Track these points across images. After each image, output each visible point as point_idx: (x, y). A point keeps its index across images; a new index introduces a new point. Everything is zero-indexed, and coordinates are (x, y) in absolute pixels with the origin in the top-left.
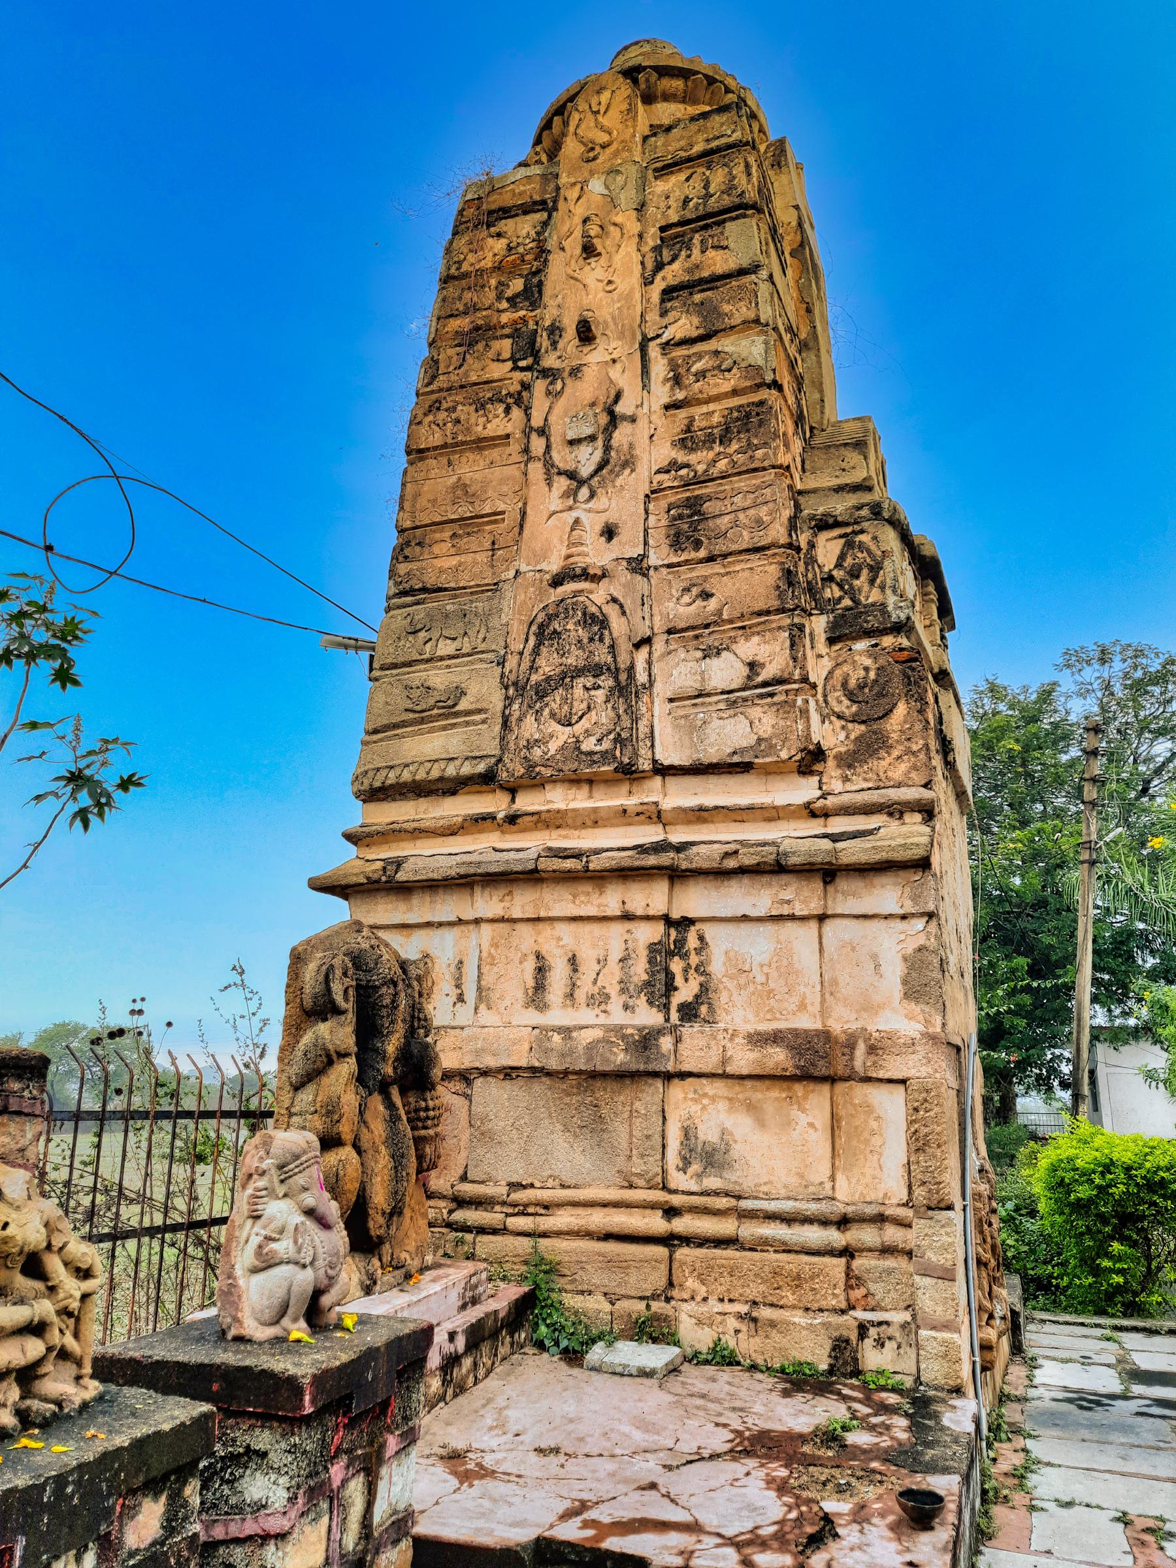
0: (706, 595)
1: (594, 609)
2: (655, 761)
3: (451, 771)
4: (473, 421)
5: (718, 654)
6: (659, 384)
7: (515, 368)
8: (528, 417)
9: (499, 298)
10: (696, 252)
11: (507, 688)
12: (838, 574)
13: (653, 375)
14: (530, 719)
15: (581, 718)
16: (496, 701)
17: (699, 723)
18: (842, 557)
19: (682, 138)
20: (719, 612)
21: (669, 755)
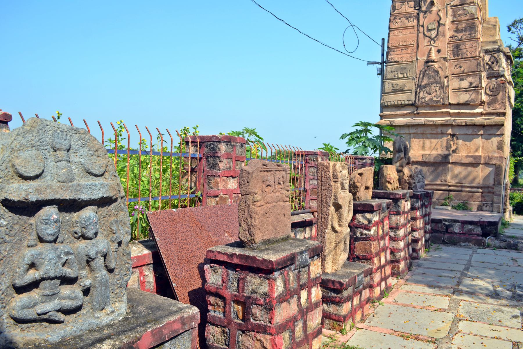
0: (461, 67)
3: (403, 102)
12: (490, 63)
13: (448, 14)
16: (414, 89)
18: (490, 59)
20: (464, 71)
21: (452, 102)
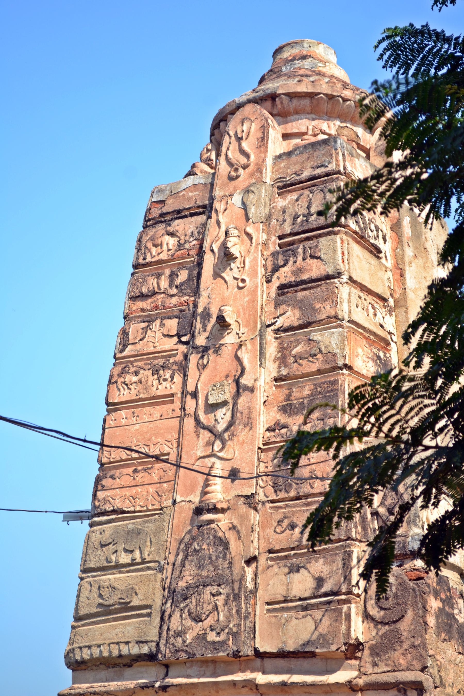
1: (220, 534)
2: (256, 650)
3: (125, 650)
4: (150, 383)
5: (298, 571)
6: (272, 362)
7: (180, 342)
8: (185, 382)
9: (171, 286)
10: (300, 258)
11: (164, 590)
14: (176, 616)
15: (208, 616)
17: (283, 621)
19: (297, 162)
